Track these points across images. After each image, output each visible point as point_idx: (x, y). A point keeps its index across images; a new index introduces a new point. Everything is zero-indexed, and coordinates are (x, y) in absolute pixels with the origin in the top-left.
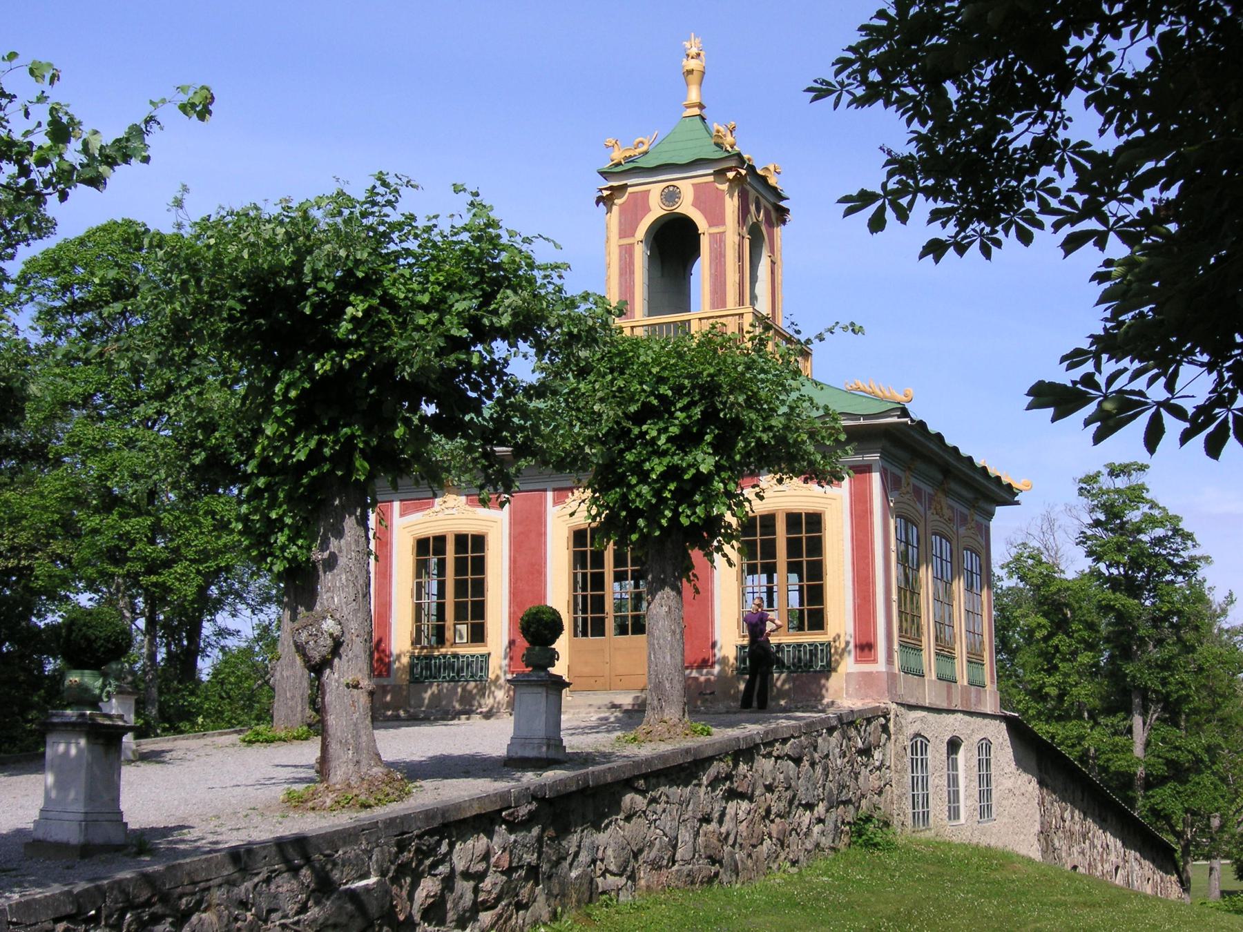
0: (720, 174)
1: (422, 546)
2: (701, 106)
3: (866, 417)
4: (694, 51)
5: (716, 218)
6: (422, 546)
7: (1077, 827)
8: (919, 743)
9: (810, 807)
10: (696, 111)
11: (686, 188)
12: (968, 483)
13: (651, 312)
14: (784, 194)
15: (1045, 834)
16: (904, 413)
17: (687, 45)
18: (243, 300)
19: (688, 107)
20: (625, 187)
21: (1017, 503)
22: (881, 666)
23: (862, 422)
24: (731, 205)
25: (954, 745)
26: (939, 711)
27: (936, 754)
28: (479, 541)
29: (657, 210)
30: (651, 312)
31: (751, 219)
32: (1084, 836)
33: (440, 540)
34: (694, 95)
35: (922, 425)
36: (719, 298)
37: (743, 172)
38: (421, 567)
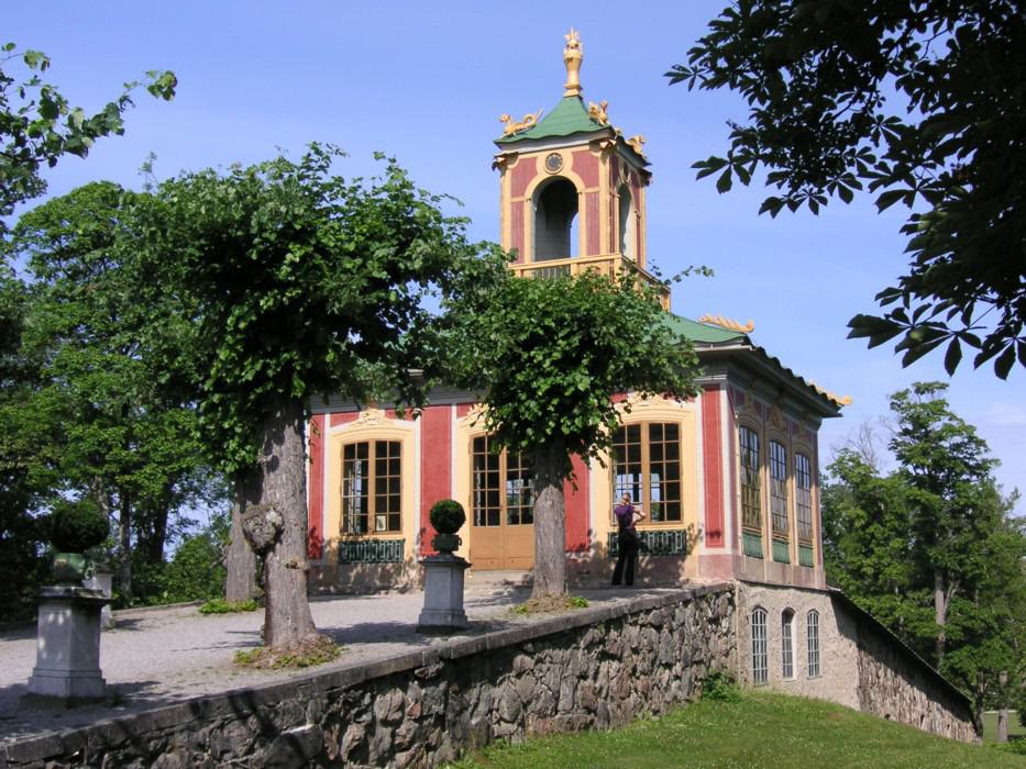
0: (595, 144)
1: (349, 450)
2: (579, 88)
3: (715, 344)
4: (573, 42)
5: (592, 180)
6: (349, 450)
7: (890, 683)
8: (759, 613)
9: (669, 666)
10: (575, 92)
11: (567, 155)
12: (800, 399)
13: (538, 258)
14: (648, 160)
15: (863, 689)
16: (747, 341)
17: (568, 37)
18: (201, 248)
19: (568, 88)
20: (517, 154)
21: (840, 415)
22: (727, 550)
23: (712, 348)
24: (604, 170)
25: (788, 615)
26: (775, 587)
27: (773, 623)
28: (396, 447)
29: (542, 174)
30: (538, 258)
31: (621, 181)
32: (896, 690)
33: (364, 446)
34: (573, 79)
35: (761, 351)
36: (594, 246)
37: (614, 142)
38: (348, 468)
